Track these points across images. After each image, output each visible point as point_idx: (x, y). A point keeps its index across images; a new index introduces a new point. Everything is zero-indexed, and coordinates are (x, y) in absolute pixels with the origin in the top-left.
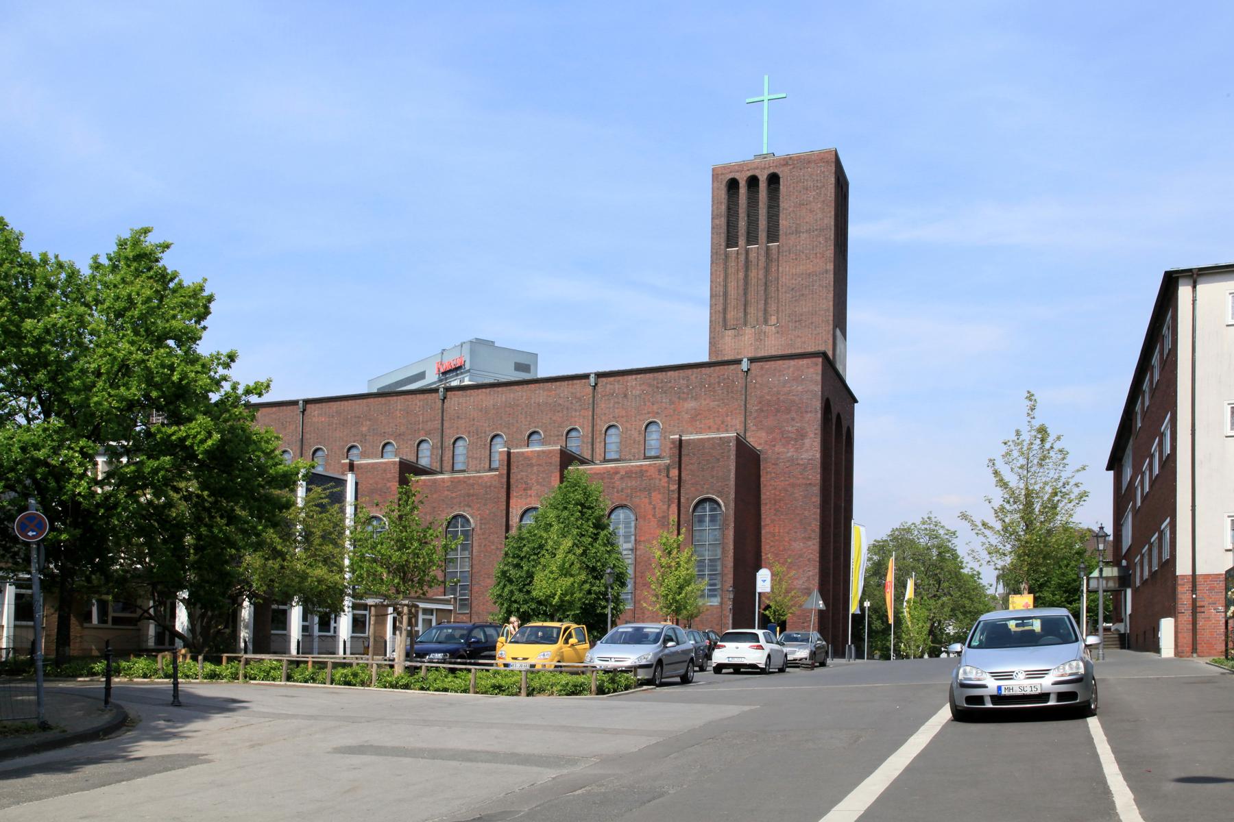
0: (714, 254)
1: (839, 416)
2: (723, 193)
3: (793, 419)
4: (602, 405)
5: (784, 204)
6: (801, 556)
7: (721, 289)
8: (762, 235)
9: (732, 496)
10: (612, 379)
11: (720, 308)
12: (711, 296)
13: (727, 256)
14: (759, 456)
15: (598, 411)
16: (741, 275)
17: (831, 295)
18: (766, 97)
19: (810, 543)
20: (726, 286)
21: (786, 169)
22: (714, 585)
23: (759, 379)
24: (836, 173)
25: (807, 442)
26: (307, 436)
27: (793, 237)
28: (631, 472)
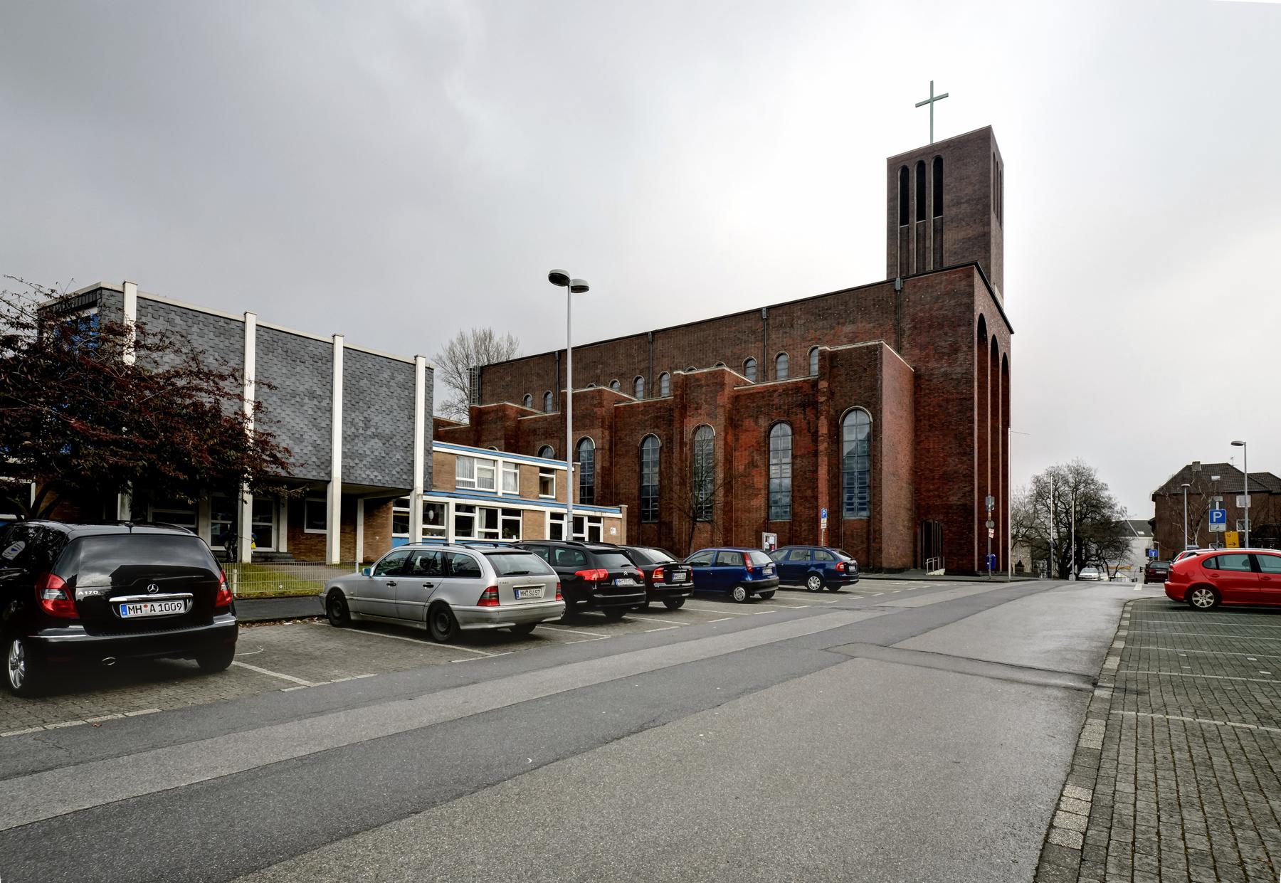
1: (994, 337)
3: (946, 334)
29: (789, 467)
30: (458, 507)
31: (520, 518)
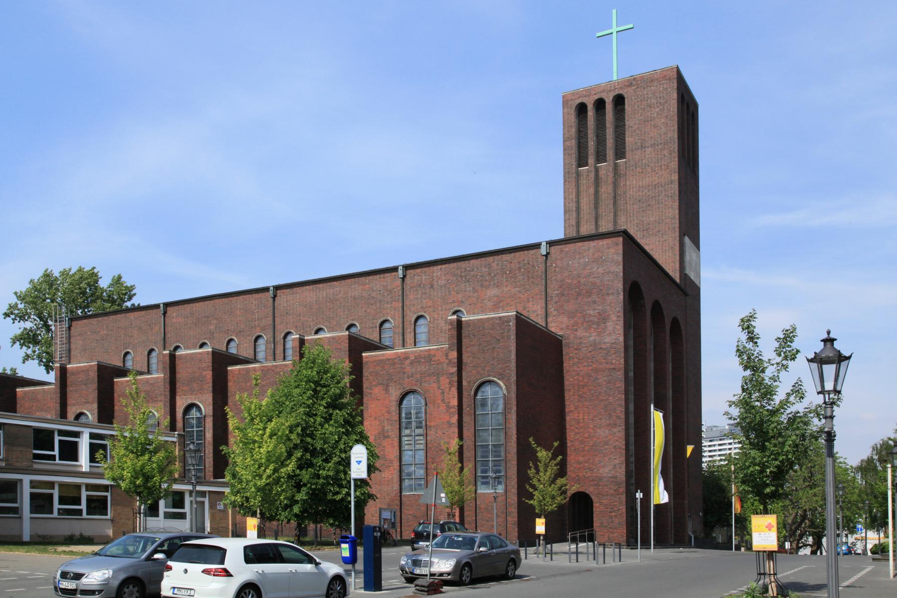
0: (567, 173)
2: (573, 118)
3: (594, 302)
4: (411, 296)
6: (607, 443)
7: (573, 206)
9: (514, 378)
12: (565, 212)
13: (578, 175)
15: (407, 302)
16: (592, 191)
17: (677, 204)
18: (614, 29)
19: (615, 430)
20: (578, 202)
21: (630, 90)
22: (499, 471)
24: (678, 89)
25: (610, 325)
26: (168, 335)
29: (581, 545)
30: (33, 484)
31: (108, 494)
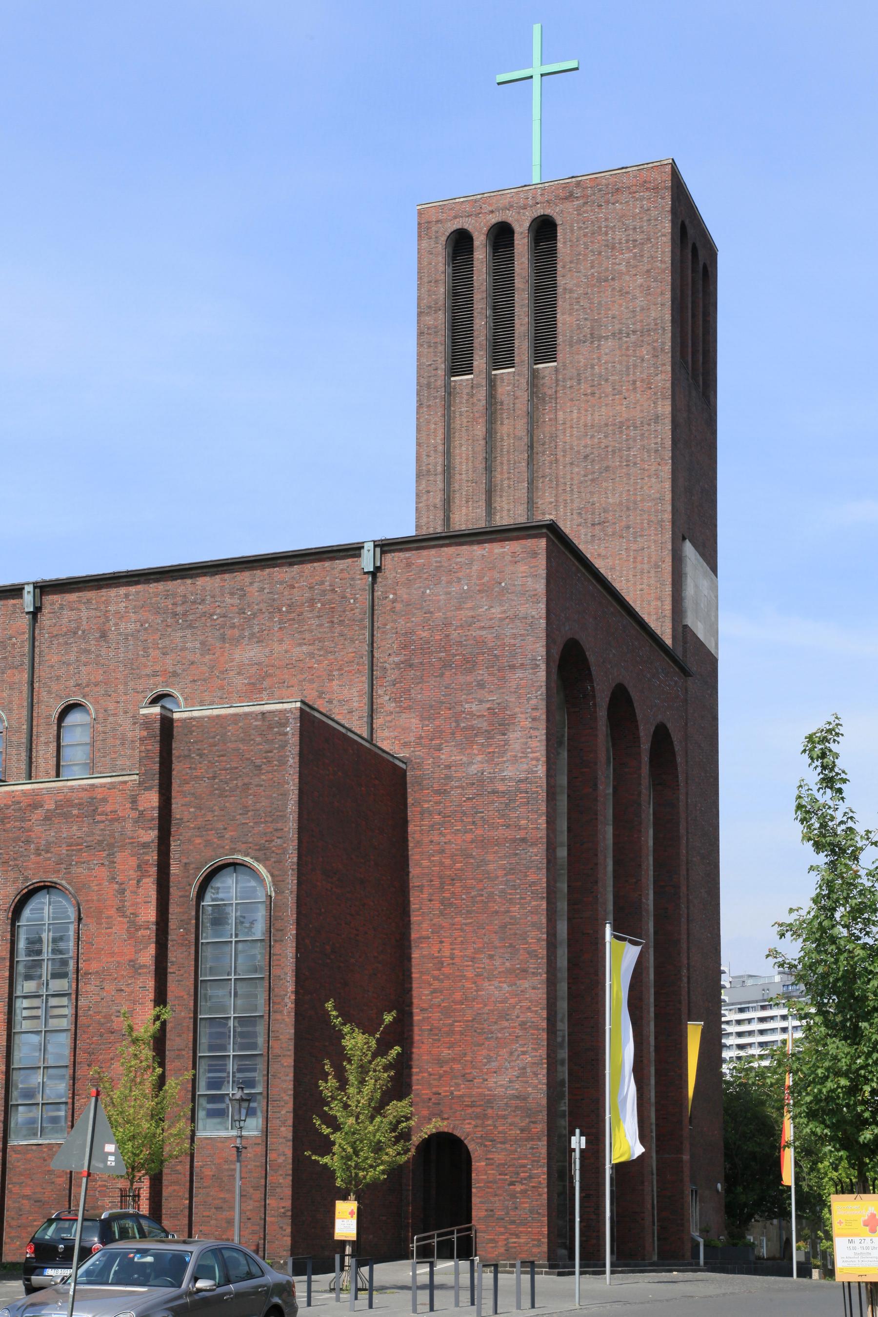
0: (424, 387)
2: (440, 262)
3: (481, 685)
4: (51, 656)
5: (565, 280)
8: (522, 347)
9: (291, 857)
10: (73, 597)
11: (437, 498)
13: (450, 392)
14: (401, 775)
16: (480, 430)
19: (526, 984)
20: (448, 454)
21: (570, 207)
22: (251, 1083)
23: (402, 592)
24: (674, 212)
25: (515, 737)
27: (585, 349)
28: (69, 802)
